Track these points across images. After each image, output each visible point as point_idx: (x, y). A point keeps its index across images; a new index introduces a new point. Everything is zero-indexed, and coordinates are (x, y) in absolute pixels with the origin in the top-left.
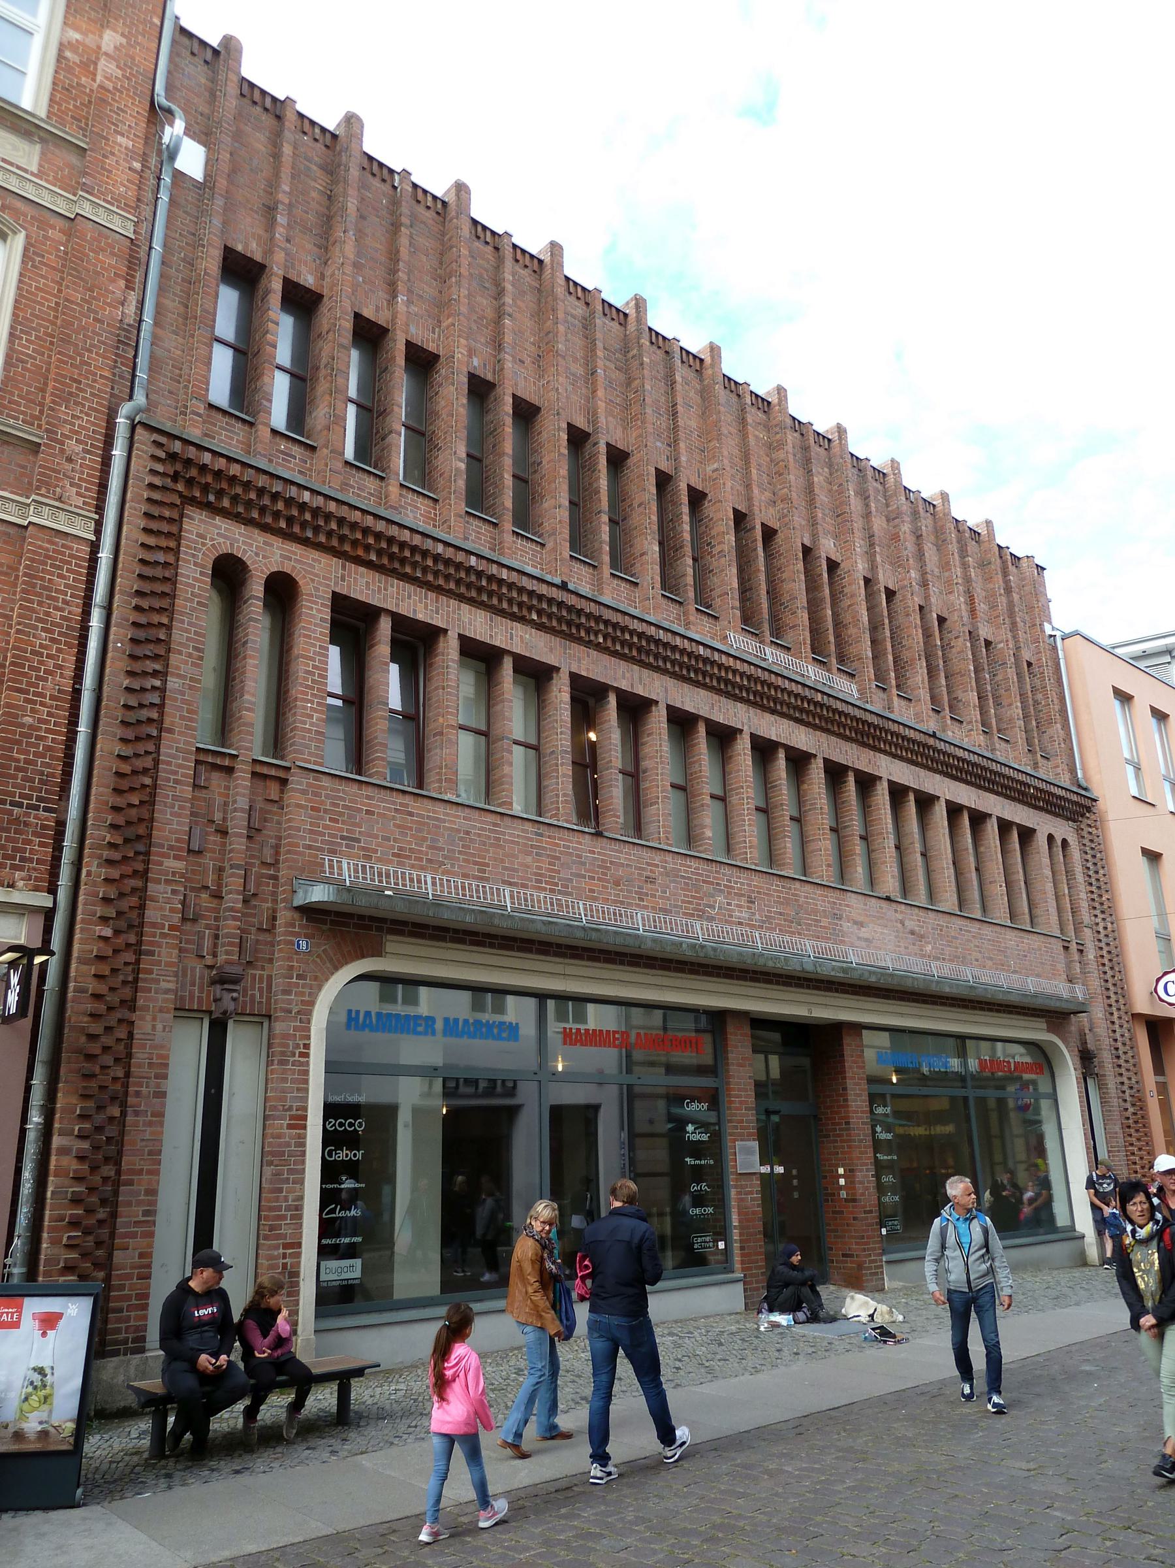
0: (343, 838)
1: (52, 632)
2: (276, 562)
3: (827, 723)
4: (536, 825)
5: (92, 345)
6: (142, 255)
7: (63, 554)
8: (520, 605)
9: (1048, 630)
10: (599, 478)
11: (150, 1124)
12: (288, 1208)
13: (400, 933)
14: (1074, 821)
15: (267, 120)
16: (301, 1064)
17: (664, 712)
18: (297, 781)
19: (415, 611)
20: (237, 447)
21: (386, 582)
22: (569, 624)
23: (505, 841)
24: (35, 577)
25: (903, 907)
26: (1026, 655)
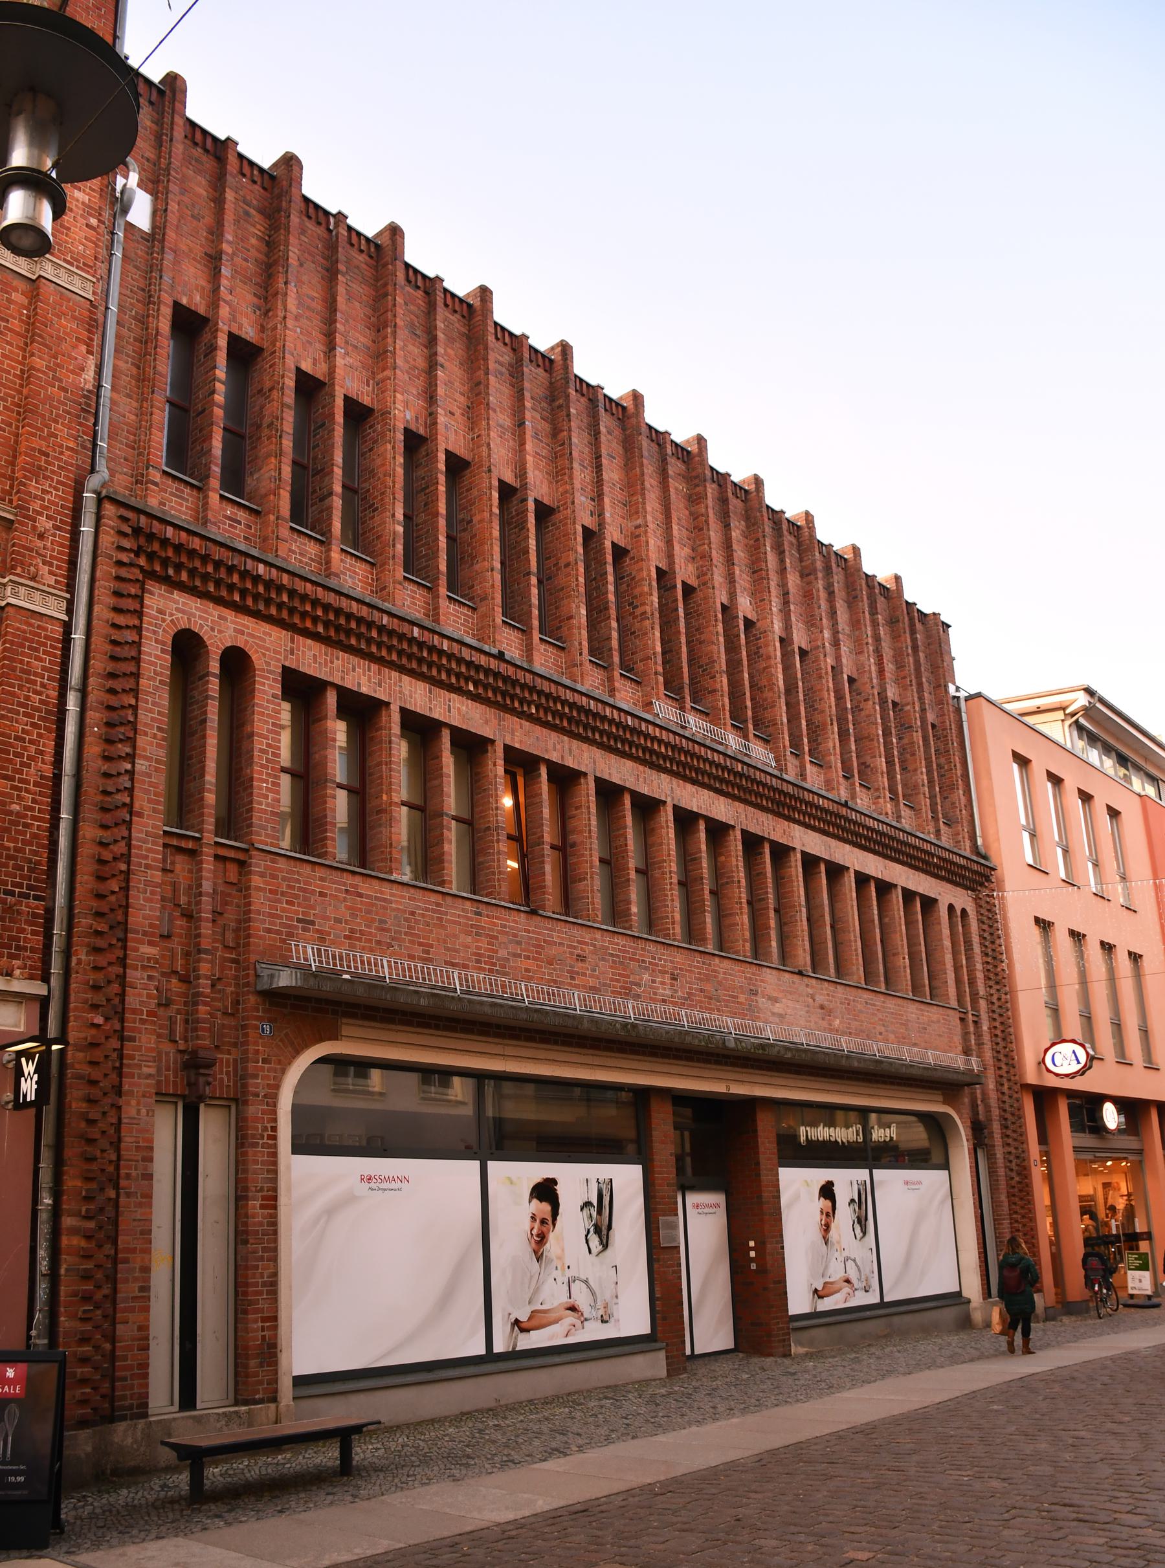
0: (299, 921)
1: (32, 717)
2: (230, 637)
3: (745, 793)
4: (476, 904)
5: (58, 415)
6: (100, 316)
7: (39, 635)
8: (458, 676)
9: (952, 689)
10: (528, 537)
11: (140, 1205)
12: (264, 1284)
13: (353, 1016)
14: (973, 890)
15: (208, 162)
16: (270, 1146)
17: (592, 785)
18: (258, 864)
19: (359, 684)
20: (186, 514)
21: (332, 654)
22: (504, 694)
23: (447, 921)
24: (14, 660)
25: (814, 981)
26: (931, 717)
